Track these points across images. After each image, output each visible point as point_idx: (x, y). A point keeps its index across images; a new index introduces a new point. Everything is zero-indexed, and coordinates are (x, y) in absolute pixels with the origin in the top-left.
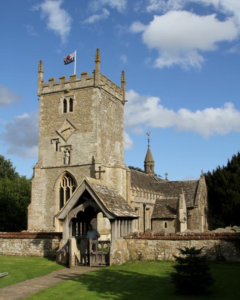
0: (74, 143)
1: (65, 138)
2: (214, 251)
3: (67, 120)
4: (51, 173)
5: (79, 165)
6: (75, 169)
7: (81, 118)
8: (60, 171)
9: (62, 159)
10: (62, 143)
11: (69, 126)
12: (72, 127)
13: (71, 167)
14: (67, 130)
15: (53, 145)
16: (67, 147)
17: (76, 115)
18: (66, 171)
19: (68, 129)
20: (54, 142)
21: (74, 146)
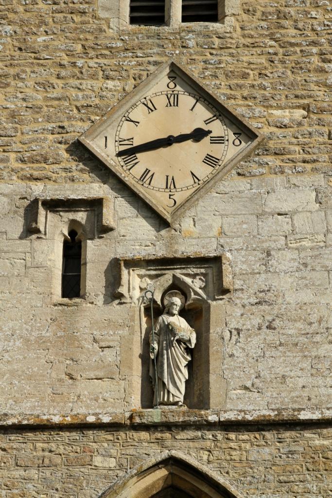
0: (238, 243)
1: (160, 201)
2: (171, 138)
3: (177, 74)
4: (20, 473)
5: (304, 416)
6: (263, 449)
7: (298, 67)
8: (112, 463)
9: (122, 364)
10: (132, 234)
11: (198, 116)
12: (218, 128)
13: (220, 435)
14: (175, 146)
15: (40, 246)
16: (178, 273)
17: (254, 45)
18: (172, 462)
19: (182, 138)
20: (55, 227)
21: (241, 267)
